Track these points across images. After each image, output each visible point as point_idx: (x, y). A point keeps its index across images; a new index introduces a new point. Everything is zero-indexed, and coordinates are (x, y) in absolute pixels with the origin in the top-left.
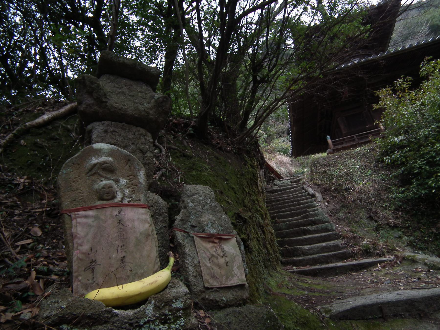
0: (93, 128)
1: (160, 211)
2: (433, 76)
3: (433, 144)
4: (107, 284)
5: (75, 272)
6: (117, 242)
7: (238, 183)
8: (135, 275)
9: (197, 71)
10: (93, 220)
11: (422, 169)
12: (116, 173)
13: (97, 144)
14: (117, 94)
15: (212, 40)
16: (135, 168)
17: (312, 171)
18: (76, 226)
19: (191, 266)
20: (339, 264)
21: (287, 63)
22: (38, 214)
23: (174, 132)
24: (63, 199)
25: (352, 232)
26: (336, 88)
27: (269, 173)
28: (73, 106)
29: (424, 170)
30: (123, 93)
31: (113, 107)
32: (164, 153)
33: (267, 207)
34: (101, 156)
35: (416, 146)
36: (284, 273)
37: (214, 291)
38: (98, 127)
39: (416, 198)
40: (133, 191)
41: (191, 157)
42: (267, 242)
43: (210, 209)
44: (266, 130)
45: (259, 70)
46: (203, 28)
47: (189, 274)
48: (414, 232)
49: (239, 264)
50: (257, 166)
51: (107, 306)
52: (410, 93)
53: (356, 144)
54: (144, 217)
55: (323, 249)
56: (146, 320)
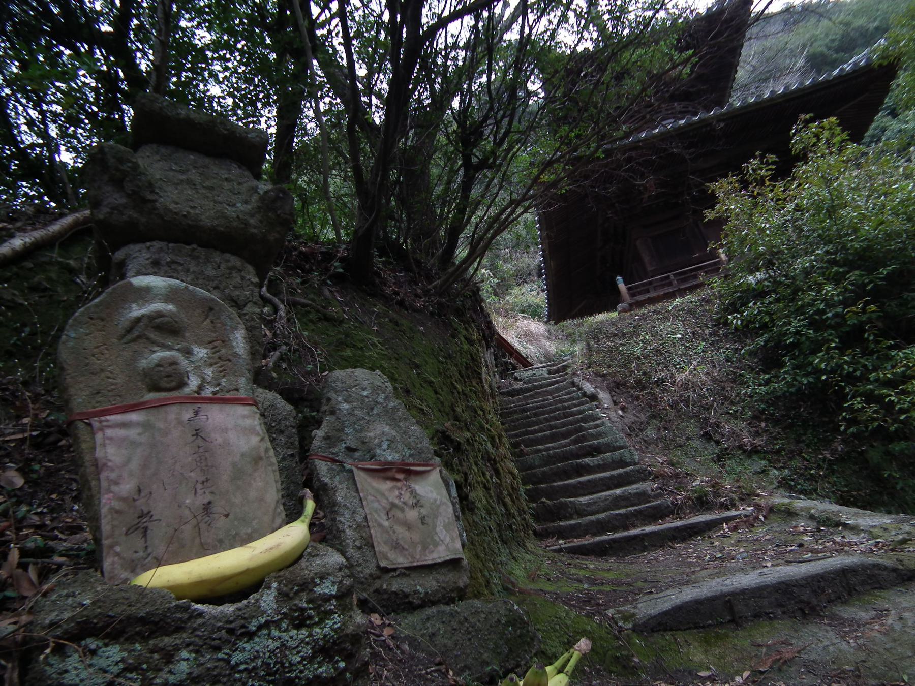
0: (128, 256)
1: (279, 423)
2: (815, 153)
3: (820, 286)
4: (179, 553)
5: (107, 538)
6: (192, 474)
7: (440, 374)
8: (234, 537)
9: (344, 147)
10: (139, 430)
11: (801, 335)
12: (183, 337)
13: (141, 278)
14: (178, 184)
15: (376, 82)
16: (224, 325)
17: (589, 348)
18: (104, 445)
19: (350, 527)
20: (648, 529)
21: (531, 128)
22: (12, 445)
23: (303, 271)
24: (72, 391)
25: (672, 466)
26: (631, 177)
27: (504, 356)
28: (78, 219)
29: (804, 338)
30: (191, 183)
31: (171, 211)
32: (282, 313)
33: (503, 424)
34: (152, 301)
35: (789, 291)
36: (541, 552)
37: (398, 576)
38: (138, 254)
39: (791, 393)
40: (223, 372)
41: (342, 322)
42: (505, 492)
43: (385, 415)
44: (493, 268)
45: (475, 144)
46: (355, 57)
47: (348, 544)
48: (791, 459)
49: (447, 521)
50: (480, 341)
51: (179, 598)
52: (774, 186)
53: (674, 292)
54: (248, 422)
55: (617, 502)
56: (263, 620)
